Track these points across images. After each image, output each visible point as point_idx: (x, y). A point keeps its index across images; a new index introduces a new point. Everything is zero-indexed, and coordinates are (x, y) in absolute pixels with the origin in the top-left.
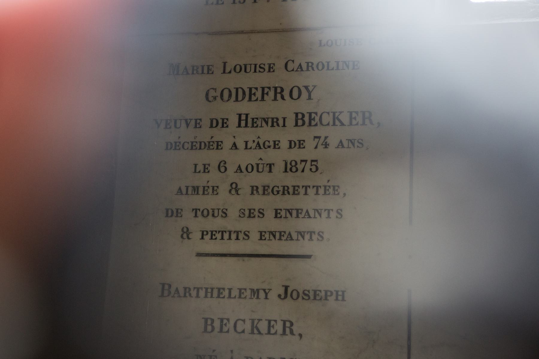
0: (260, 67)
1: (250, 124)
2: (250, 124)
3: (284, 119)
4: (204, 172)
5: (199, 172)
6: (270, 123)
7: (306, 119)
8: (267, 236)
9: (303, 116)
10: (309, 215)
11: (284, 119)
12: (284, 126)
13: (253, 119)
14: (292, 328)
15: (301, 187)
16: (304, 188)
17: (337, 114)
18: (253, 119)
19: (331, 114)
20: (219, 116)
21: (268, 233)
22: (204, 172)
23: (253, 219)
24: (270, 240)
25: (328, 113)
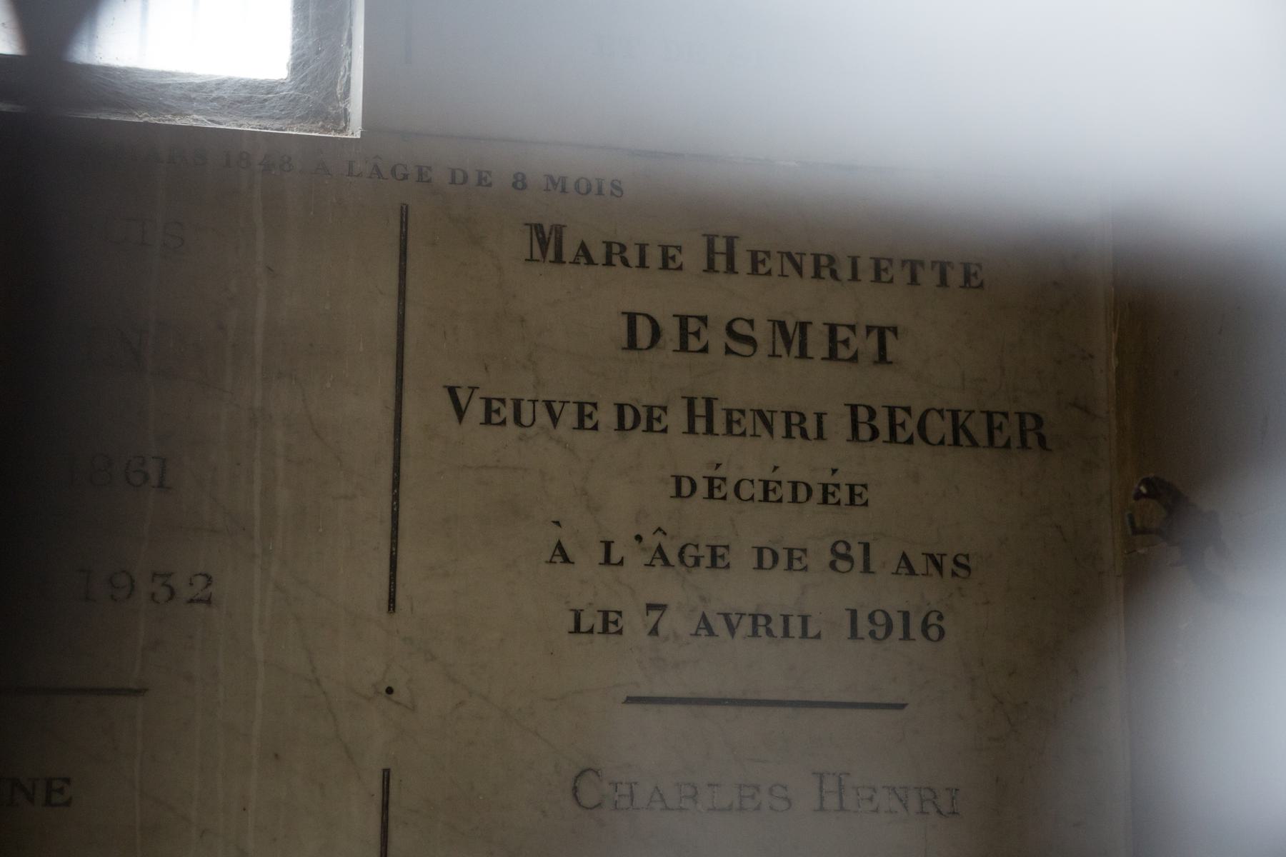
0: (750, 341)
1: (720, 425)
2: (720, 425)
3: (820, 417)
4: (605, 630)
5: (591, 631)
6: (779, 428)
7: (882, 422)
8: (747, 422)
9: (872, 413)
10: (909, 566)
11: (820, 417)
12: (820, 436)
13: (729, 412)
14: (834, 267)
15: (861, 331)
16: (874, 335)
17: (962, 416)
18: (729, 412)
19: (948, 415)
20: (638, 438)
21: (749, 415)
22: (605, 630)
23: (677, 272)
24: (754, 435)
25: (940, 412)
